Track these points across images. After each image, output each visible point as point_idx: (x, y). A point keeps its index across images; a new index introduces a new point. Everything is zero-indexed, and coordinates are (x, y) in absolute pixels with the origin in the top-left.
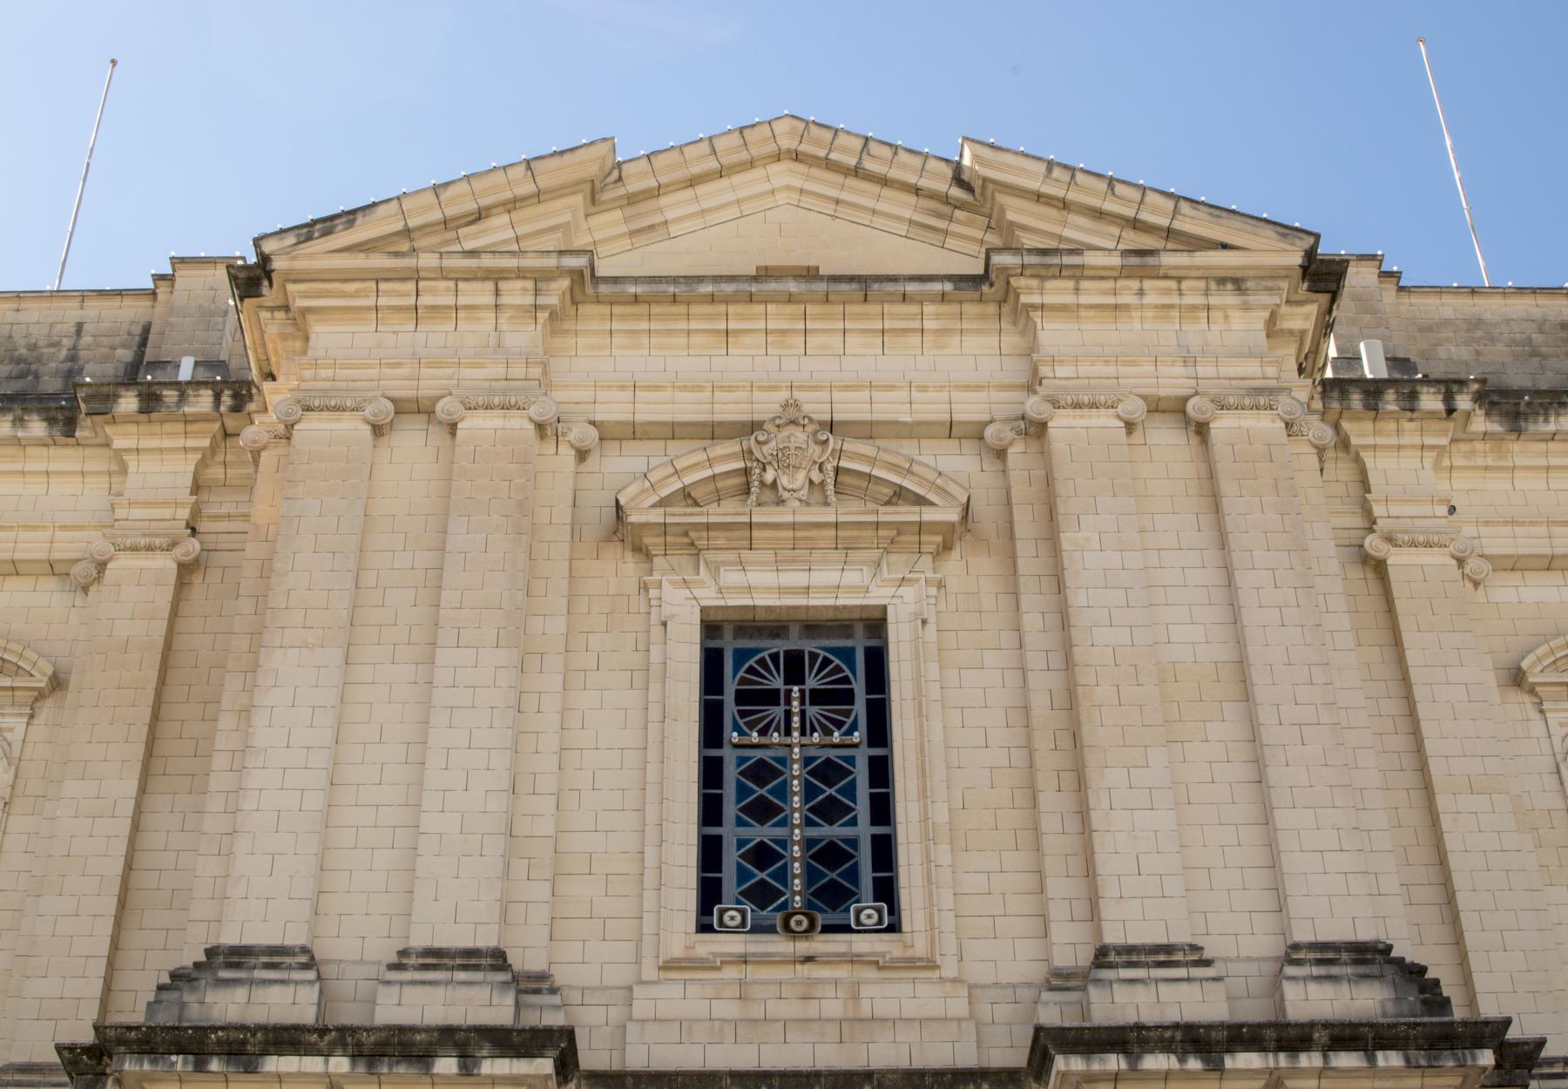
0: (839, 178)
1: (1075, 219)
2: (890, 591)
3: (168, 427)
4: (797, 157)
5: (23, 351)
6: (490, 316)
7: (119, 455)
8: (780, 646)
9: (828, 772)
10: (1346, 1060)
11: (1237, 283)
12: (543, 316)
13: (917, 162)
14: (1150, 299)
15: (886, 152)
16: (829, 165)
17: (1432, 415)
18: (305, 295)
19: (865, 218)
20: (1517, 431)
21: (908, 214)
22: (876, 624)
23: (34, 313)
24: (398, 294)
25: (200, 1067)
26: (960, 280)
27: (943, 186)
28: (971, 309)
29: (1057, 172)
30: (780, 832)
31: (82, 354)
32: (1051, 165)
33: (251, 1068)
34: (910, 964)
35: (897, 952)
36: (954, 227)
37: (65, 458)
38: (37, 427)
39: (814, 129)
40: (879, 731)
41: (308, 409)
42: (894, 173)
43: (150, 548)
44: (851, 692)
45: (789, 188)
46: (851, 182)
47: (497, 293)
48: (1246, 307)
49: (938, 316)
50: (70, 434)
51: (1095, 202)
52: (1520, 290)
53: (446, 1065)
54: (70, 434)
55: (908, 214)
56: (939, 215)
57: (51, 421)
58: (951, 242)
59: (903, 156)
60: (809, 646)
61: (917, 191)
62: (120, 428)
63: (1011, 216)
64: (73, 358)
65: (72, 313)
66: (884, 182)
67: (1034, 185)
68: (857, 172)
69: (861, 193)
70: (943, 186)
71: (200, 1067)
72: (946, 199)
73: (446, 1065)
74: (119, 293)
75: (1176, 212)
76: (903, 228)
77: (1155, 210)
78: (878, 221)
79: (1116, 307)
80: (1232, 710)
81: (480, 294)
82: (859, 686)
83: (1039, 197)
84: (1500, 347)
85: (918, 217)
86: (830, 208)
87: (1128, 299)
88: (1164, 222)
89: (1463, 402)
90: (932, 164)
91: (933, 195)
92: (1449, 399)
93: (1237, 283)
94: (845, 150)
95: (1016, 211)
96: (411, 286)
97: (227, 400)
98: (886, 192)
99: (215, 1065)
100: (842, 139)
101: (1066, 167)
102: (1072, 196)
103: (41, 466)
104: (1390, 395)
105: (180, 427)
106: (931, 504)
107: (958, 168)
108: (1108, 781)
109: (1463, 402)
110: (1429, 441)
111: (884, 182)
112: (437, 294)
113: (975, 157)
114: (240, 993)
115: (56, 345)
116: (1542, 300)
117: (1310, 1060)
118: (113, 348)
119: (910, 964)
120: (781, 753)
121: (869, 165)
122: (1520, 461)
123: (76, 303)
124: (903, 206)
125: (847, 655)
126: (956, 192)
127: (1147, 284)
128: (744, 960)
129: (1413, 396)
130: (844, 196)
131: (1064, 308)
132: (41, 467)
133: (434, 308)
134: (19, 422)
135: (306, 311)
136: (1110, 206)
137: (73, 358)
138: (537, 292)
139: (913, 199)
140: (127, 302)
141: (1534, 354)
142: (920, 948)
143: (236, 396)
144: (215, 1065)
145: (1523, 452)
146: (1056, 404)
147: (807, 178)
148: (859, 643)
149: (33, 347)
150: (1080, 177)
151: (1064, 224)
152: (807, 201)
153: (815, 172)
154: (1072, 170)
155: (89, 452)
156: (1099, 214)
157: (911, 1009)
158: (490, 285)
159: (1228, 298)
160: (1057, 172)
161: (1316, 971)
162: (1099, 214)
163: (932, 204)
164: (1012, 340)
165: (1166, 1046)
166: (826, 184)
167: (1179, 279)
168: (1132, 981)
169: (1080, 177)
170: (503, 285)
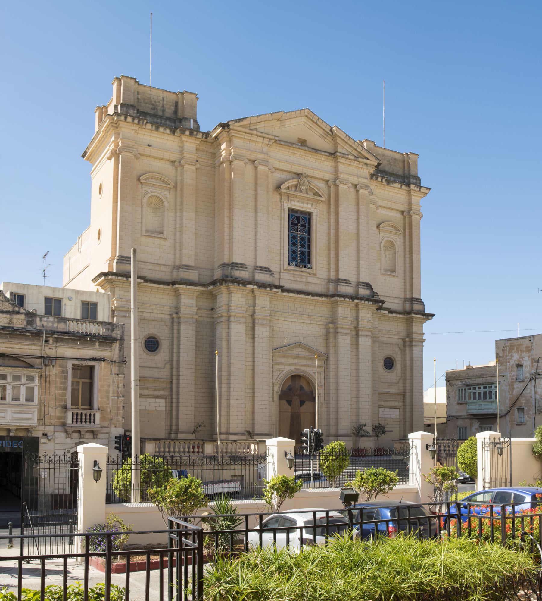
0: (312, 122)
1: (347, 145)
2: (313, 210)
3: (193, 138)
4: (307, 116)
5: (153, 102)
6: (261, 144)
7: (183, 141)
8: (297, 215)
9: (302, 239)
10: (366, 302)
11: (367, 165)
12: (269, 145)
13: (325, 125)
14: (355, 164)
15: (321, 121)
16: (312, 120)
17: (379, 181)
18: (234, 133)
19: (314, 131)
20: (388, 185)
21: (321, 133)
22: (310, 214)
23: (154, 92)
24: (248, 137)
25: (239, 285)
26: (329, 153)
27: (328, 131)
28: (329, 158)
29: (347, 137)
30: (296, 248)
31: (165, 106)
32: (347, 135)
33: (245, 286)
34: (313, 274)
35: (312, 272)
36: (327, 138)
37: (171, 138)
38: (168, 131)
39: (311, 113)
40: (309, 234)
41: (236, 159)
42: (322, 126)
43: (192, 165)
44: (306, 225)
45: (304, 121)
46: (314, 124)
47: (263, 140)
48: (367, 169)
49: (324, 158)
50: (174, 133)
51: (351, 144)
52: (391, 150)
53: (268, 289)
54: (174, 133)
55: (321, 133)
56: (326, 135)
57: (171, 130)
58: (326, 140)
59: (324, 123)
60: (301, 216)
61: (324, 130)
62: (184, 136)
63: (338, 141)
64: (163, 107)
65: (161, 95)
66: (319, 126)
67: (343, 138)
68: (316, 123)
69: (314, 126)
70: (328, 131)
71: (239, 285)
72: (328, 133)
73: (268, 289)
74: (170, 92)
75: (362, 150)
76: (319, 135)
77: (359, 149)
78: (316, 132)
79: (350, 165)
80: (355, 242)
81: (260, 140)
82: (307, 224)
83: (343, 140)
84: (386, 162)
85: (322, 134)
86: (309, 127)
87: (352, 164)
88: (360, 151)
89: (384, 180)
90: (328, 126)
91: (326, 131)
92: (382, 180)
93: (367, 165)
94: (315, 119)
95: (339, 141)
96: (250, 135)
97: (204, 136)
98: (319, 128)
99: (241, 285)
100: (315, 116)
101: (349, 136)
102: (348, 142)
103: (167, 138)
104: (375, 177)
105: (195, 138)
106: (321, 197)
107: (331, 128)
108: (342, 253)
109: (384, 180)
110: (377, 185)
111: (319, 126)
112: (254, 138)
113: (336, 130)
114: (238, 272)
115: (159, 102)
116: (393, 153)
117: (363, 302)
118: (170, 106)
119: (313, 274)
120: (297, 235)
121: (318, 123)
122: (386, 189)
123: (161, 92)
124: (321, 131)
125: (305, 218)
126: (330, 133)
127: (356, 162)
128: (294, 270)
129: (377, 178)
130: (312, 126)
131: (343, 163)
132: (167, 138)
133: (253, 140)
134: (165, 129)
135: (232, 136)
136: (353, 146)
137: (163, 107)
138: (269, 141)
139: (322, 130)
140: (171, 94)
141: (390, 164)
142: (314, 272)
143: (206, 136)
144: (241, 285)
145: (387, 188)
146: (341, 183)
147: (307, 120)
148: (307, 217)
149: (155, 102)
150: (350, 139)
151: (345, 145)
152: (306, 125)
153: (309, 120)
154: (349, 137)
155: (176, 137)
156: (351, 146)
157: (313, 282)
158: (262, 138)
159: (365, 167)
160: (347, 137)
161: (362, 287)
162: (351, 146)
163: (325, 133)
164: (333, 164)
165: (348, 298)
166: (309, 123)
167: (360, 162)
168: (343, 285)
169: (350, 139)
170: (264, 139)
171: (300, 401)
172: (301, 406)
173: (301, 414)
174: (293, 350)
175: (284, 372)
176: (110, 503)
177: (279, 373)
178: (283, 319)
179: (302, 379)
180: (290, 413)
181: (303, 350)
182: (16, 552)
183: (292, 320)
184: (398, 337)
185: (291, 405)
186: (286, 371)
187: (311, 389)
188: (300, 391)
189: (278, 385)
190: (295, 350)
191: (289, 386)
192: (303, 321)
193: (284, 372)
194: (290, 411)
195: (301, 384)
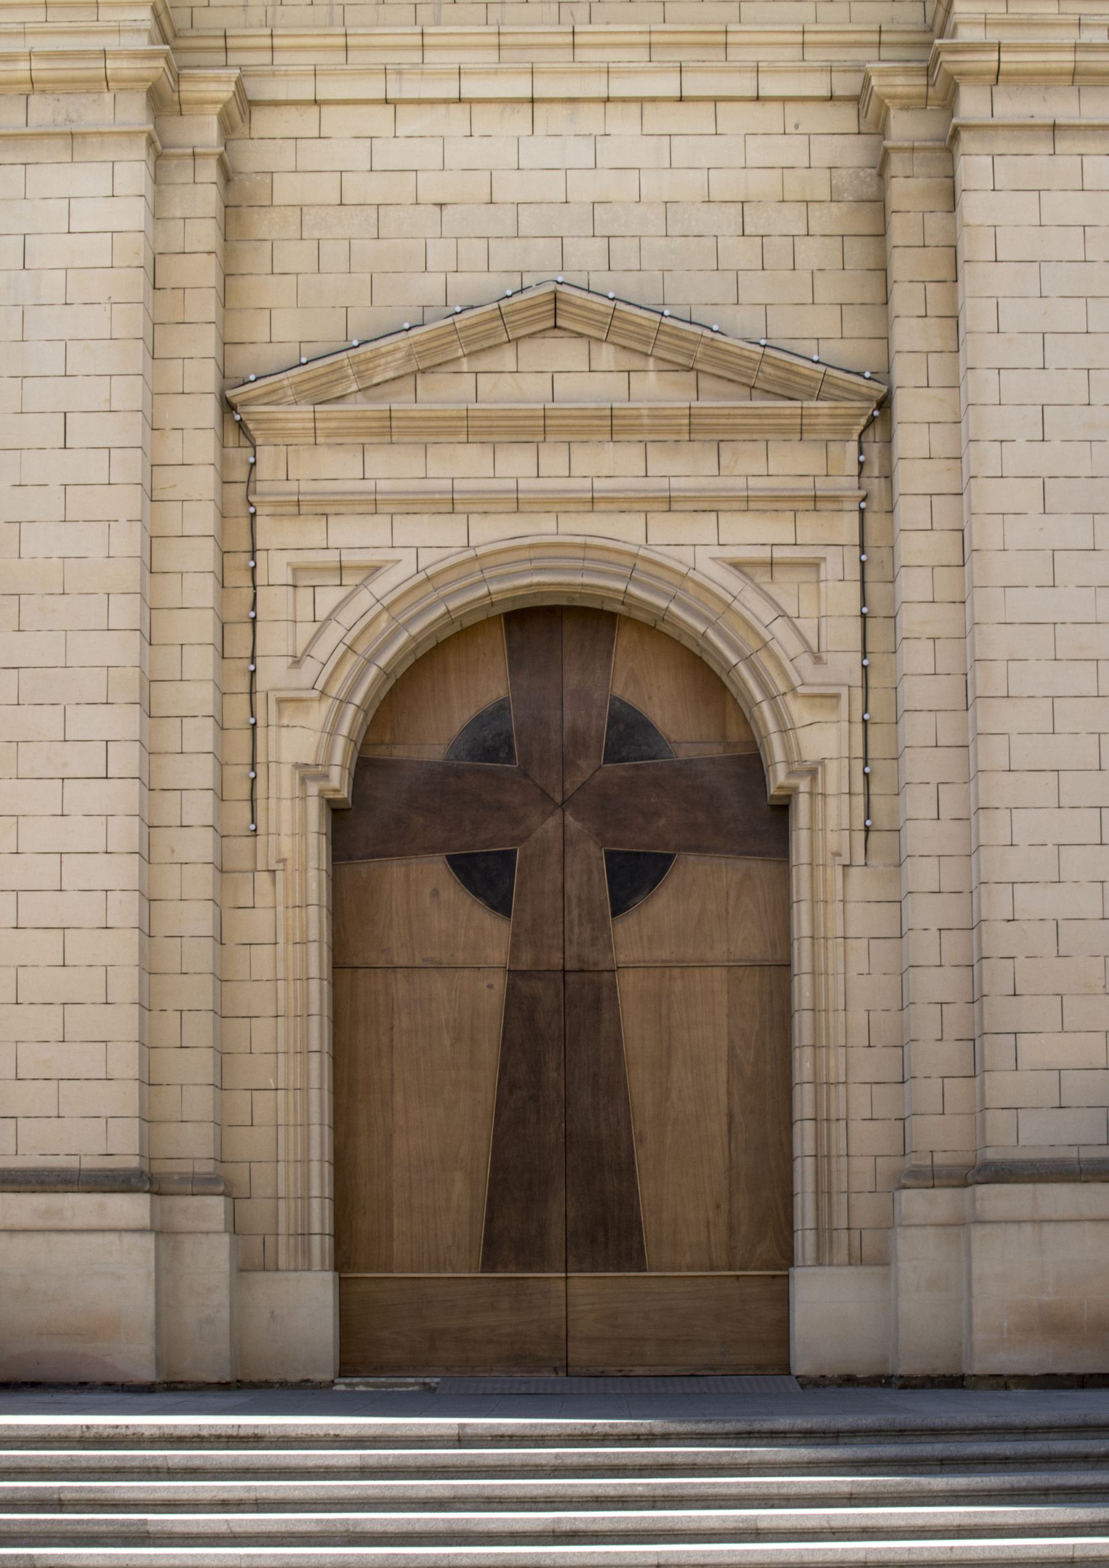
171: (610, 856)
172: (619, 907)
173: (628, 984)
174: (486, 362)
175: (382, 585)
176: (633, 1227)
177: (329, 598)
178: (373, 88)
179: (624, 640)
180: (499, 982)
181: (606, 356)
182: (844, 1234)
183: (472, 88)
184: (817, 86)
185: (501, 905)
186: (407, 568)
187: (735, 732)
188: (613, 755)
189: (319, 713)
190: (506, 359)
191: (480, 721)
192: (596, 87)
193: (382, 585)
194: (498, 954)
195: (618, 691)
